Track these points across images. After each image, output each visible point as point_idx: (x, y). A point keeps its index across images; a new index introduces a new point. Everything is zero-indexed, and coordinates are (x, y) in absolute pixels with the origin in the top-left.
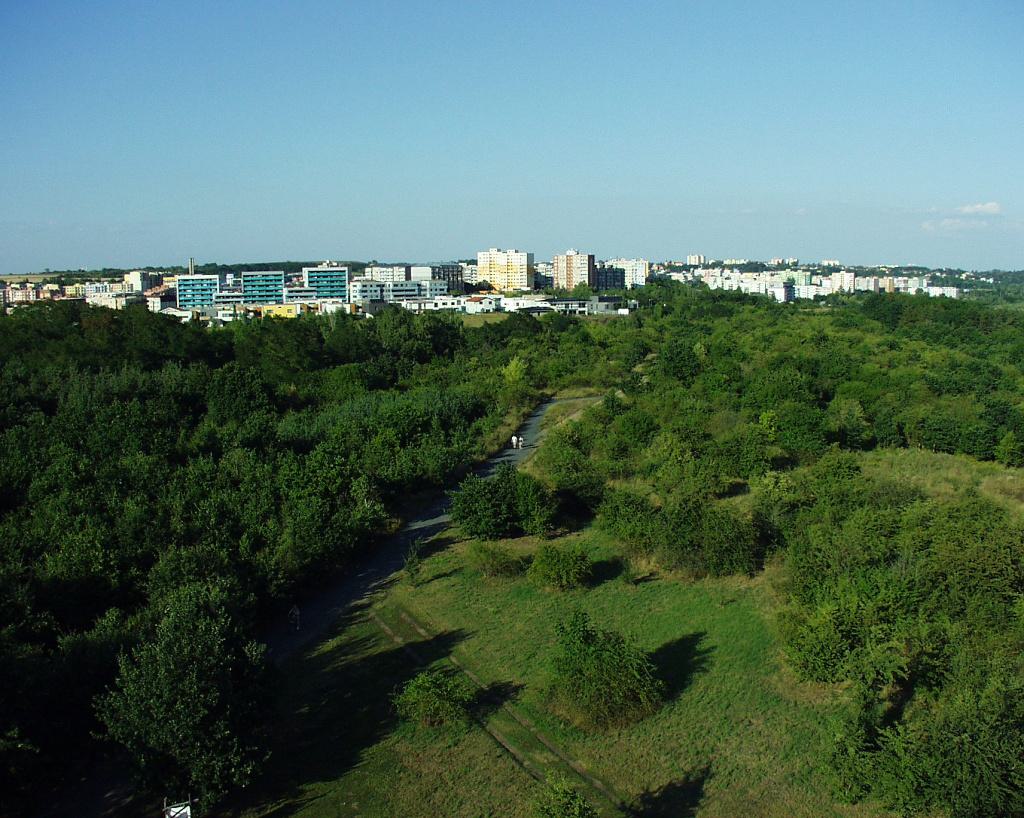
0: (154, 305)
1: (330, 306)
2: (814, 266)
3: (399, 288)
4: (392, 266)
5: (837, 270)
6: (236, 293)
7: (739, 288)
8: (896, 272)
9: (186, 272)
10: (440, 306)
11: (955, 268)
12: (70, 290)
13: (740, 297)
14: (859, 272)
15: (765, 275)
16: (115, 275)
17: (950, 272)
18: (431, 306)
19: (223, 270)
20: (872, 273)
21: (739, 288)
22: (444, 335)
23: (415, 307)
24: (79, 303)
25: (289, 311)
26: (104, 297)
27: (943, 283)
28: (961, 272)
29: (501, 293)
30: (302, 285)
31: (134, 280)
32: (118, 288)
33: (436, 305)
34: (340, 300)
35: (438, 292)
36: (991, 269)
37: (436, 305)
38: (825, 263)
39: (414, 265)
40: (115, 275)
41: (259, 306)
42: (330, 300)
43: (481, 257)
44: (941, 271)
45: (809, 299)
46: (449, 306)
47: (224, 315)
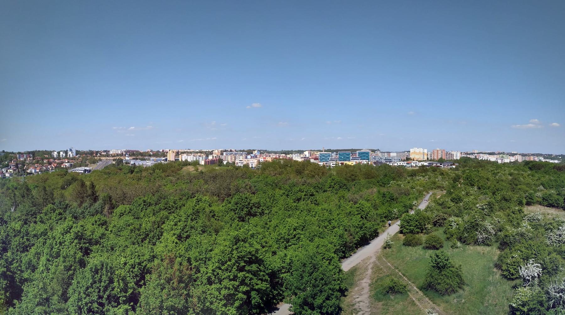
0: (312, 161)
1: (365, 162)
2: (509, 153)
3: (387, 159)
4: (384, 153)
5: (516, 154)
6: (336, 158)
7: (487, 159)
8: (533, 155)
9: (322, 151)
10: (399, 164)
11: (550, 154)
12: (288, 156)
13: (488, 162)
14: (523, 155)
15: (495, 156)
16: (301, 152)
17: (549, 155)
18: (396, 164)
19: (332, 151)
20: (513, 155)
21: (487, 159)
22: (399, 173)
23: (392, 164)
24: (291, 159)
25: (352, 163)
26: (298, 158)
27: (547, 158)
28: (552, 155)
29: (417, 161)
30: (356, 156)
31: (307, 153)
32: (302, 156)
33: (398, 164)
34: (367, 161)
35: (399, 160)
36: (560, 154)
37: (398, 164)
38: (513, 152)
39: (391, 152)
40: (301, 152)
41: (343, 162)
42: (364, 161)
43: (412, 150)
44: (546, 155)
45: (508, 163)
46: (401, 164)
47: (333, 164)
